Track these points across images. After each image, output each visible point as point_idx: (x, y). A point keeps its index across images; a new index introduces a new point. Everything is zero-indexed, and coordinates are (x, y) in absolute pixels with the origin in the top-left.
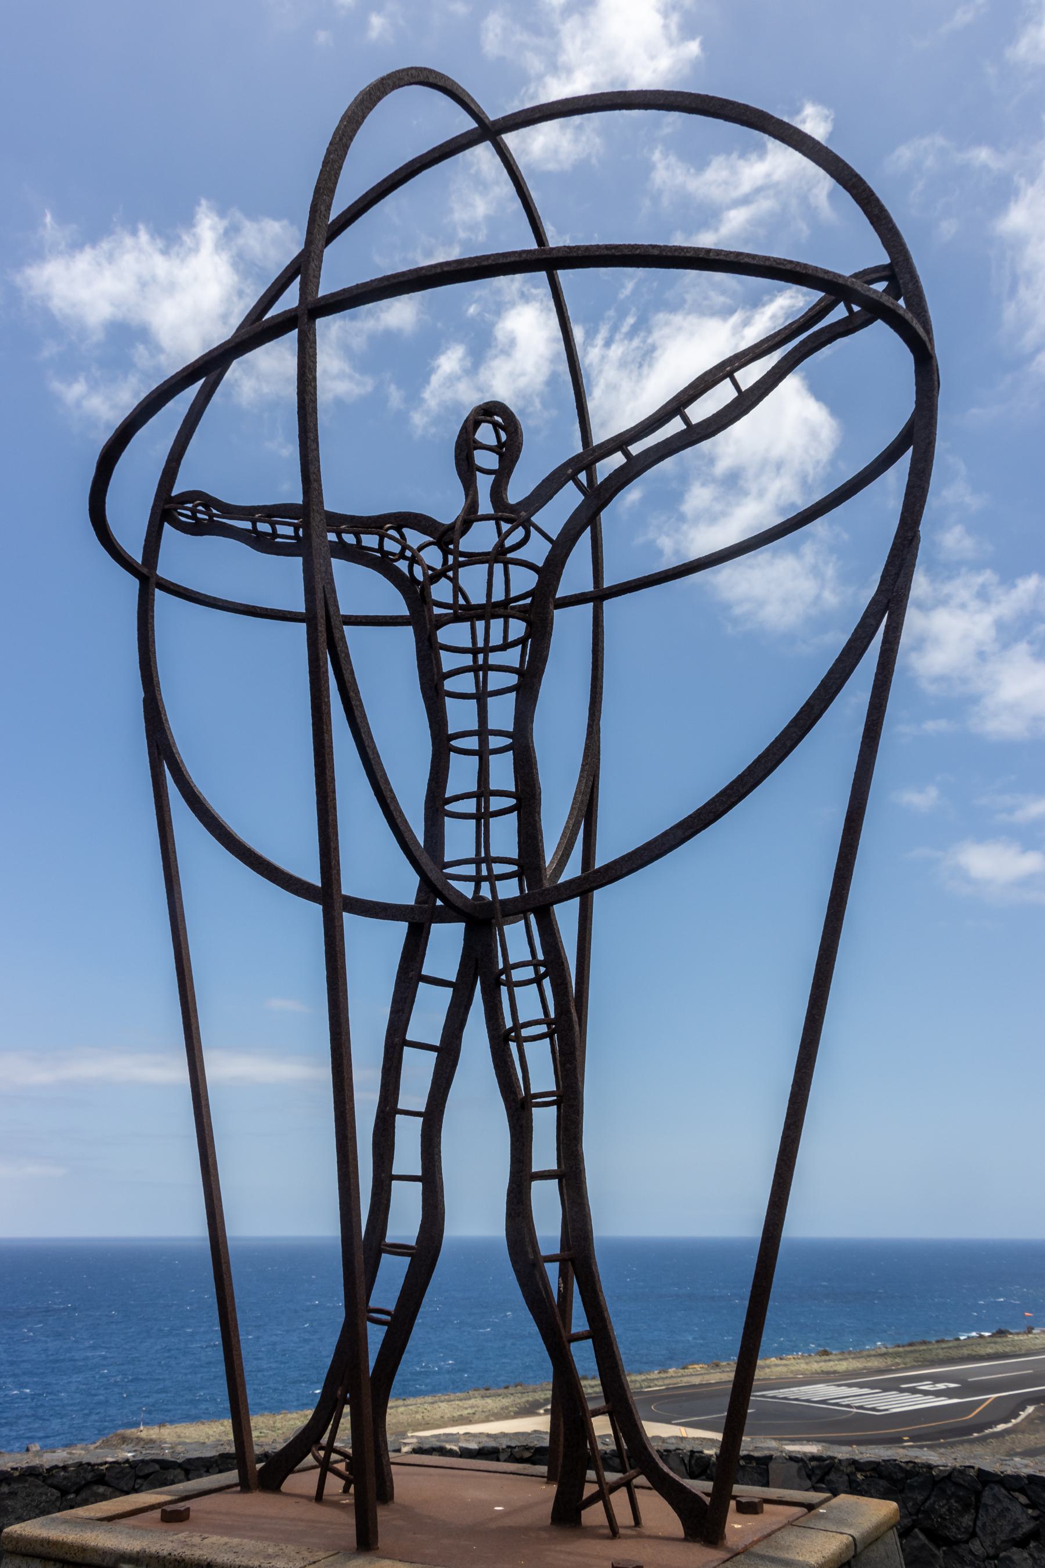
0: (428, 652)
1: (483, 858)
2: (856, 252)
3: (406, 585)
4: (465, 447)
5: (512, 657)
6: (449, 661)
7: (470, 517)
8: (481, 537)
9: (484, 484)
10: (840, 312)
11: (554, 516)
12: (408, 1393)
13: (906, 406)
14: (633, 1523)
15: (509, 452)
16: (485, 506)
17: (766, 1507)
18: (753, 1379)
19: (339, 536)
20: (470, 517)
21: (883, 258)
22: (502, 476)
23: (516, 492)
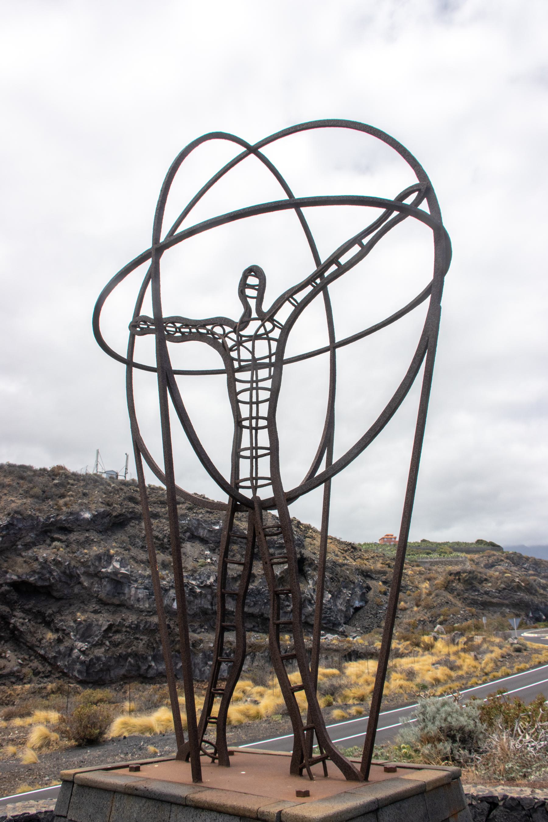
0: (232, 382)
1: (254, 478)
2: (394, 180)
3: (224, 351)
4: (243, 285)
5: (268, 384)
6: (239, 387)
7: (245, 321)
8: (251, 329)
9: (252, 303)
10: (395, 213)
11: (282, 316)
12: (243, 679)
13: (428, 277)
14: (323, 774)
15: (261, 289)
16: (254, 315)
17: (397, 769)
18: (363, 755)
19: (197, 330)
20: (245, 321)
21: (414, 180)
22: (260, 299)
23: (266, 307)
